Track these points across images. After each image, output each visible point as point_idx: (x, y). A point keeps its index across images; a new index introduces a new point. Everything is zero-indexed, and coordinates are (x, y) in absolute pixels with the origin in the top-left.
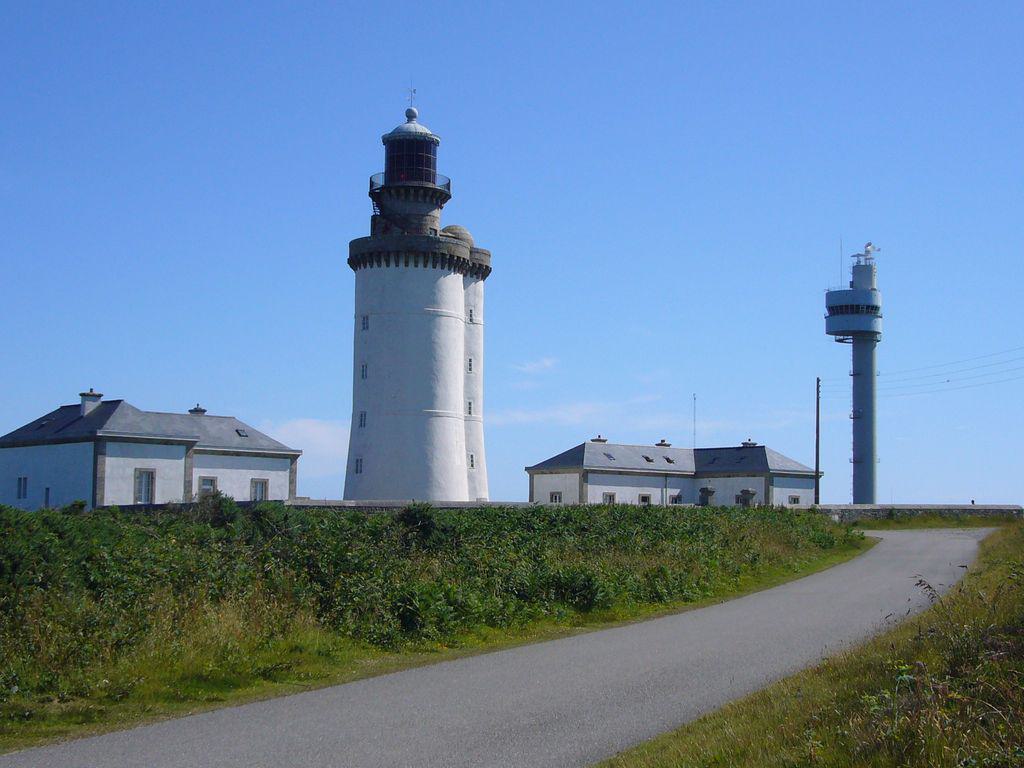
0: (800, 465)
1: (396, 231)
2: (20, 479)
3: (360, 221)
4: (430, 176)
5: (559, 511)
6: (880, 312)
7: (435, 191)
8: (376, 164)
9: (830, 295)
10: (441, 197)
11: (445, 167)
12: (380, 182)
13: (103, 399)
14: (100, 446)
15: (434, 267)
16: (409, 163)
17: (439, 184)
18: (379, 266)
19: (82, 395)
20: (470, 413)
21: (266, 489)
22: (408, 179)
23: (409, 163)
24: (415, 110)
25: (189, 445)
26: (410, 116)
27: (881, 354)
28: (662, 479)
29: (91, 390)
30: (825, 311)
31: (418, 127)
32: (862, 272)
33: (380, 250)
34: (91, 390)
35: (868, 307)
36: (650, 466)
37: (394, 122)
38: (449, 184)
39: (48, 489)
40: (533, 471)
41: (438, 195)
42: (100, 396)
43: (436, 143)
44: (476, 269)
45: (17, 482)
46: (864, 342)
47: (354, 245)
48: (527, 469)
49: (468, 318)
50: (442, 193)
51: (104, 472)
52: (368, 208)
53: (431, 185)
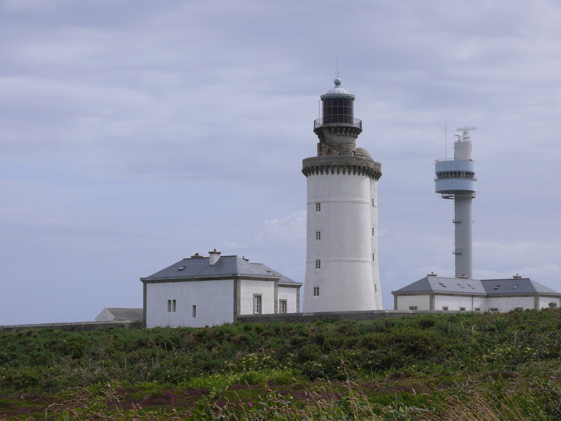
0: (550, 289)
1: (335, 153)
2: (170, 301)
3: (311, 146)
4: (349, 119)
5: (446, 315)
6: (475, 176)
7: (353, 128)
8: (316, 113)
9: (438, 164)
10: (357, 131)
11: (359, 113)
12: (321, 123)
13: (221, 255)
14: (236, 278)
15: (349, 174)
16: (337, 114)
17: (355, 124)
18: (327, 173)
19: (210, 253)
20: (373, 260)
21: (286, 305)
22: (341, 121)
23: (337, 114)
24: (340, 79)
25: (276, 280)
26: (337, 83)
27: (475, 206)
28: (470, 298)
29: (215, 250)
30: (435, 176)
31: (343, 90)
32: (462, 147)
33: (328, 164)
34: (215, 250)
35: (467, 173)
36: (444, 289)
37: (329, 89)
38: (361, 123)
39: (195, 307)
40: (397, 294)
41: (354, 130)
42: (220, 253)
43: (353, 99)
44: (375, 174)
45: (320, 294)
46: (462, 197)
47: (305, 161)
48: (392, 292)
49: (372, 203)
50: (356, 129)
51: (240, 296)
52: (316, 139)
53: (348, 125)
